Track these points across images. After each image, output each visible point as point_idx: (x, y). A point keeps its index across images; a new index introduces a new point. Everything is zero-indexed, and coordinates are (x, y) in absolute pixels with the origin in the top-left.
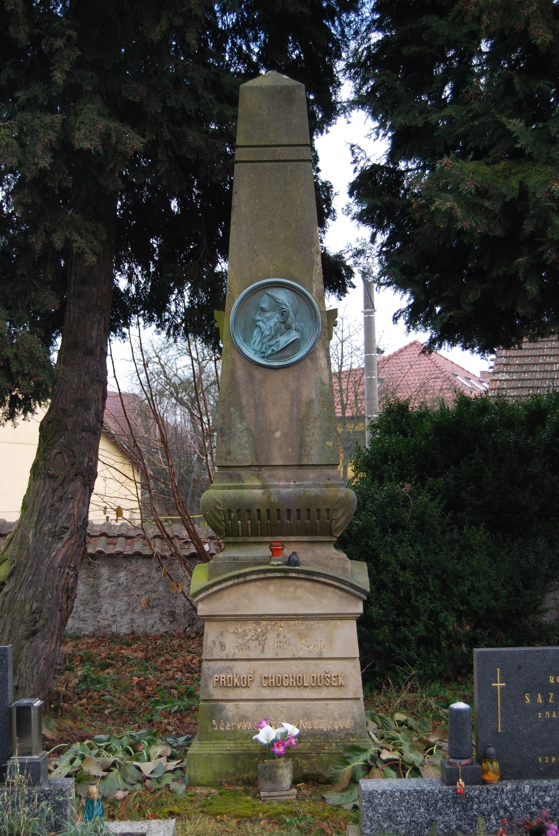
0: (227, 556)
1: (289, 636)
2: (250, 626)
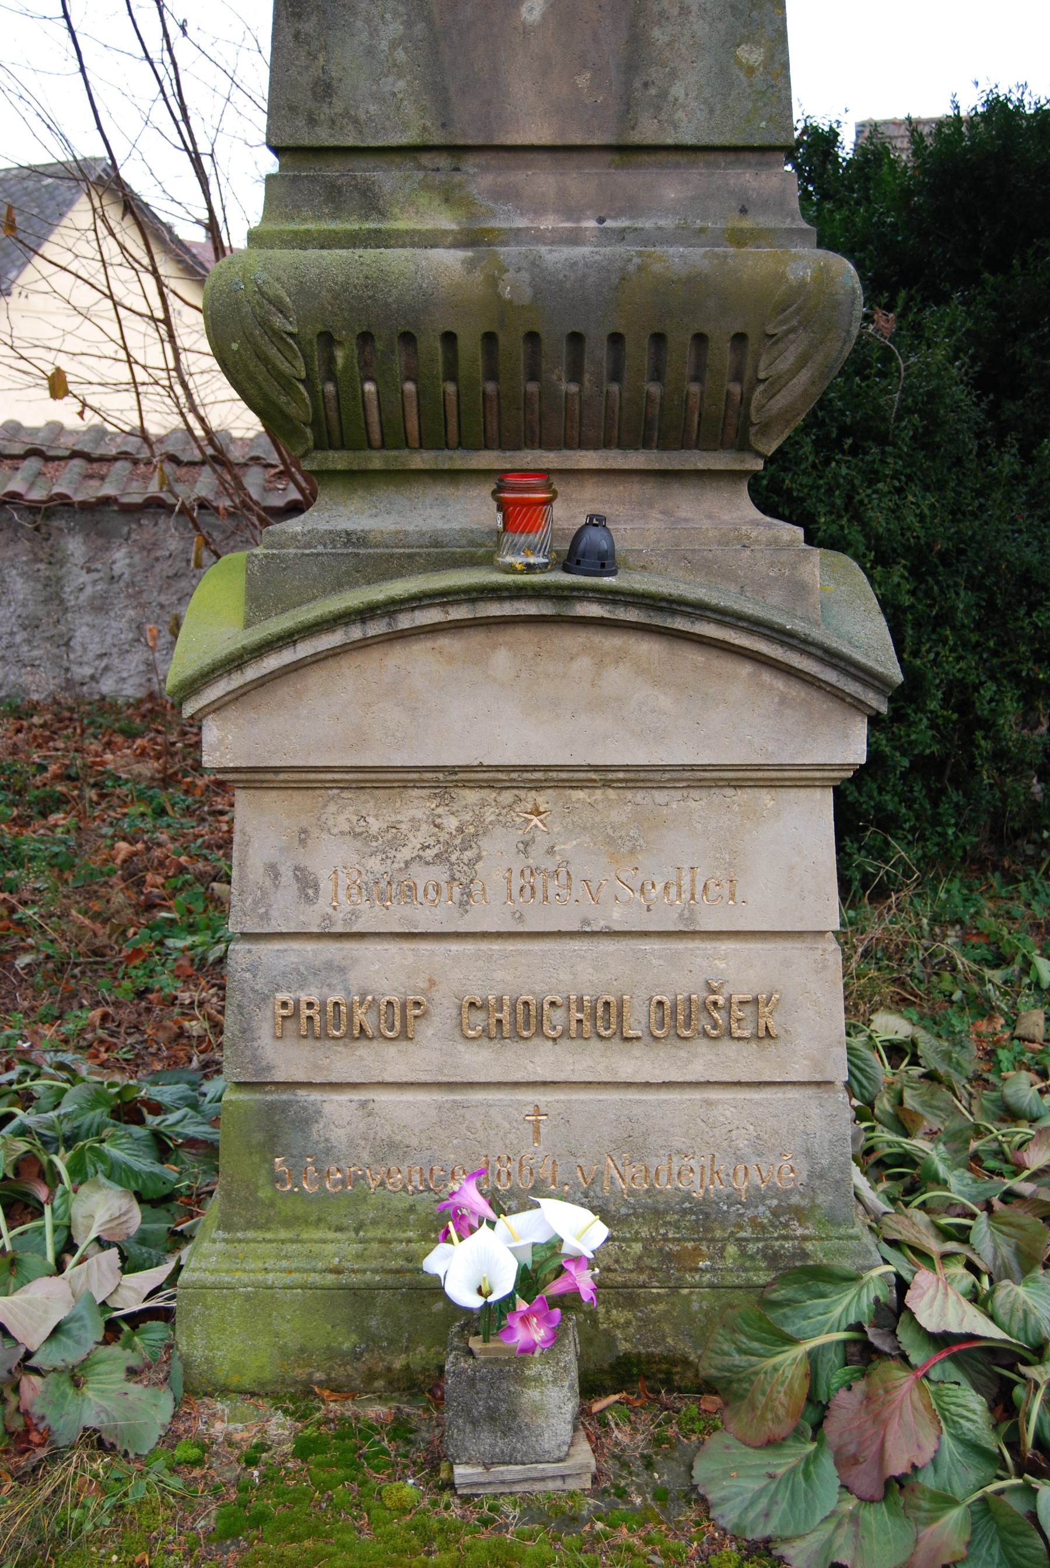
0: (323, 527)
1: (567, 847)
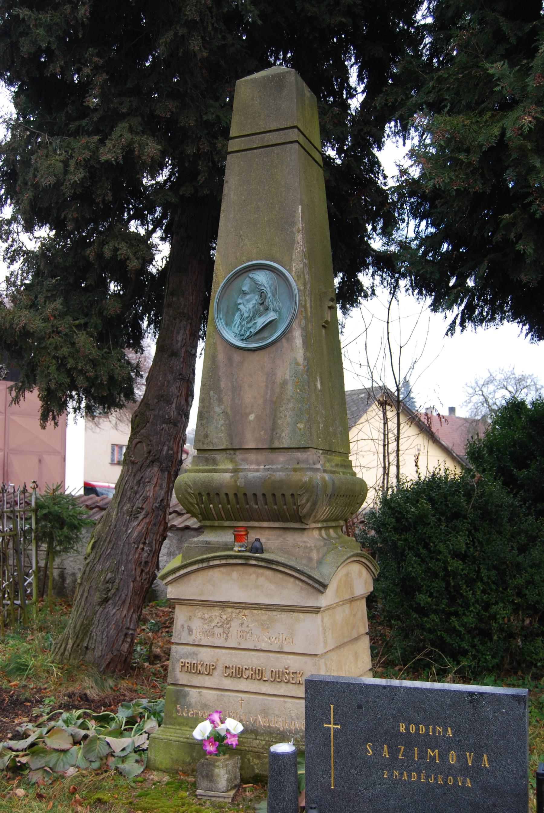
1: (252, 625)
2: (216, 612)
